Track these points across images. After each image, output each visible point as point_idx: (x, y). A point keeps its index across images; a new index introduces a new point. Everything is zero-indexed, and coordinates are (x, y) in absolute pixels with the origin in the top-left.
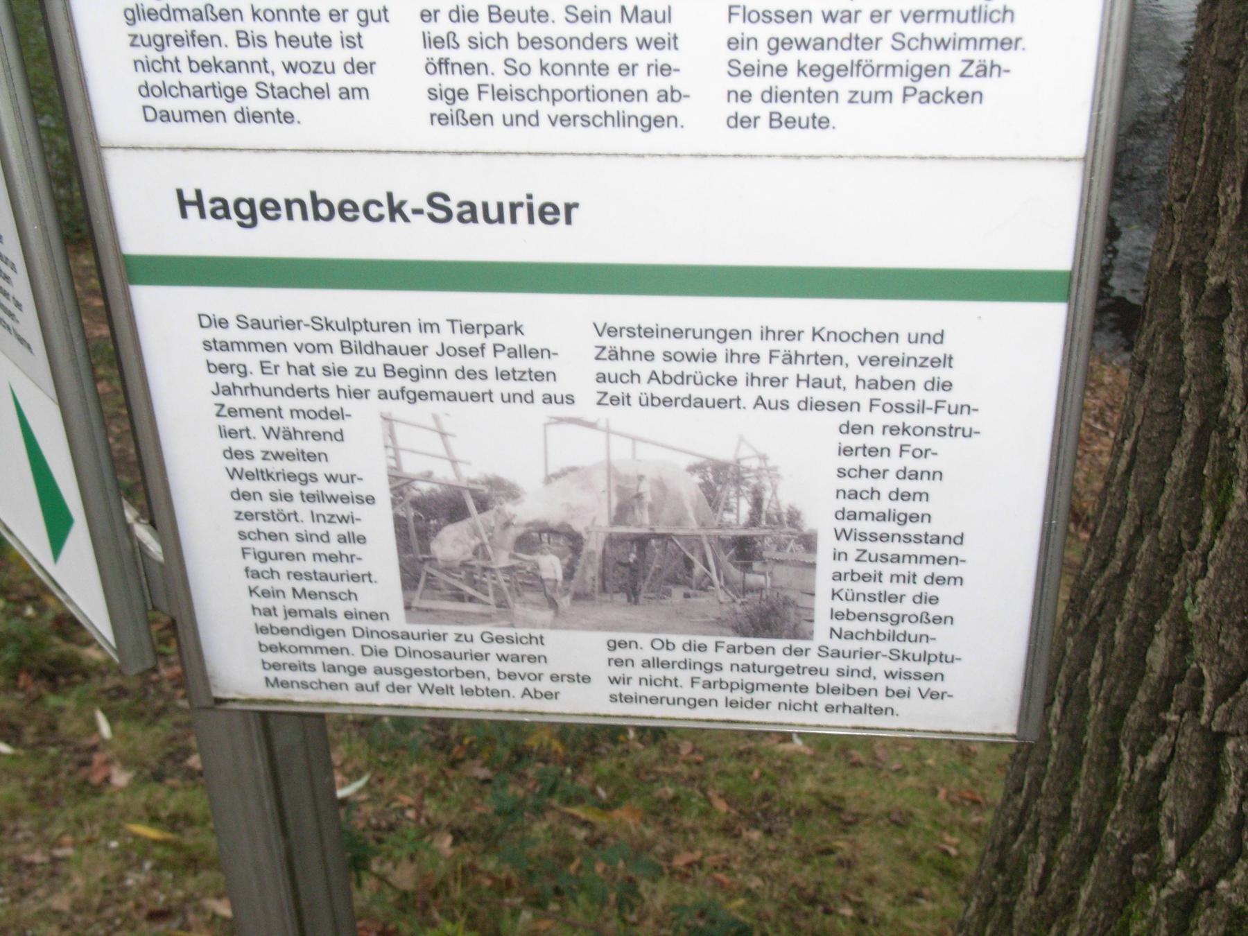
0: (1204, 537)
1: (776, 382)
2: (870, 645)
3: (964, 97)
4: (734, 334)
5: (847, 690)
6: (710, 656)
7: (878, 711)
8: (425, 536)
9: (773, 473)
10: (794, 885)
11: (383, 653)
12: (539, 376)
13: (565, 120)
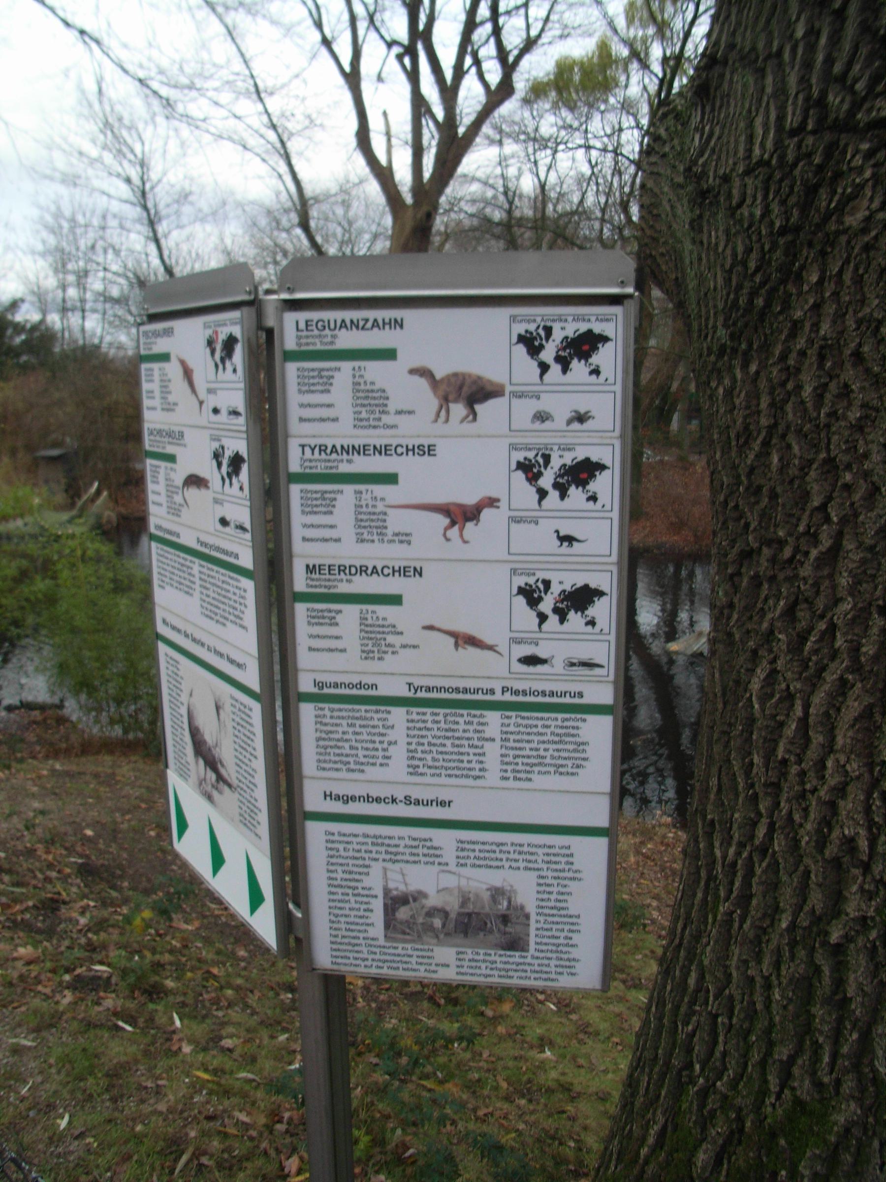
0: (709, 927)
1: (516, 861)
2: (549, 955)
3: (573, 774)
4: (502, 844)
5: (541, 972)
6: (493, 958)
7: (553, 980)
8: (394, 910)
9: (515, 892)
10: (543, 1129)
11: (375, 953)
12: (437, 856)
13: (450, 776)
